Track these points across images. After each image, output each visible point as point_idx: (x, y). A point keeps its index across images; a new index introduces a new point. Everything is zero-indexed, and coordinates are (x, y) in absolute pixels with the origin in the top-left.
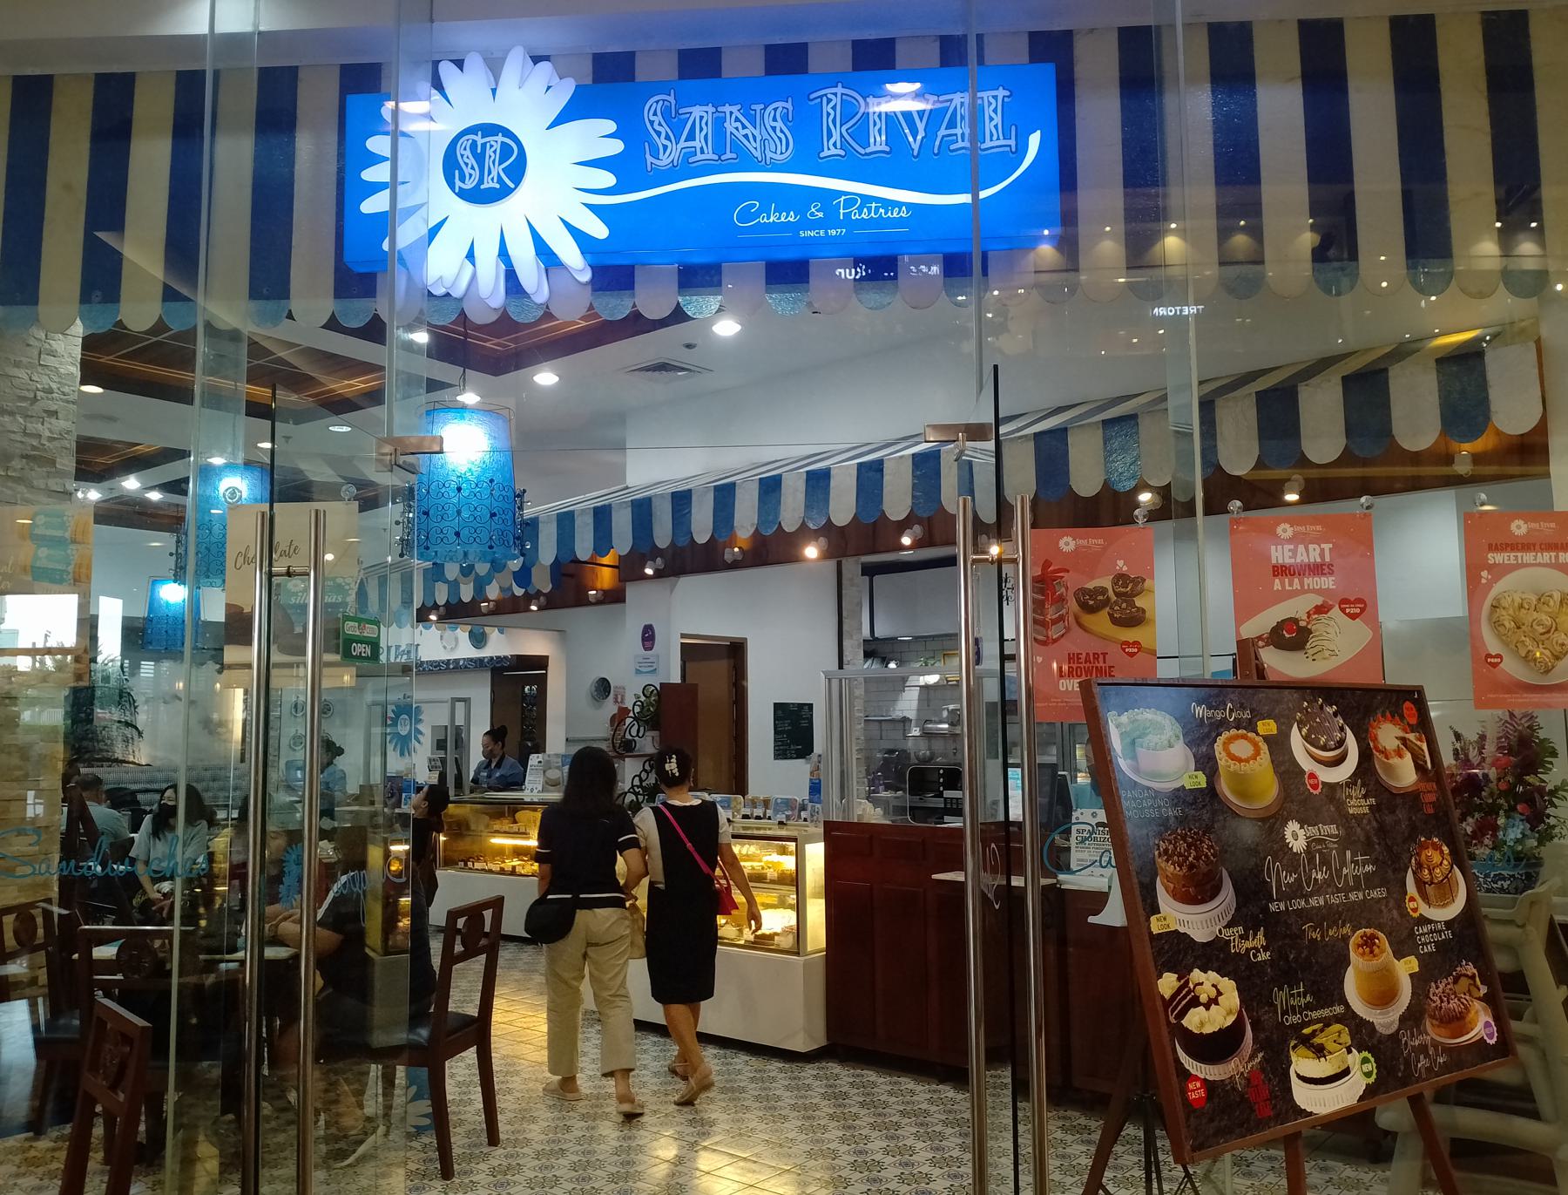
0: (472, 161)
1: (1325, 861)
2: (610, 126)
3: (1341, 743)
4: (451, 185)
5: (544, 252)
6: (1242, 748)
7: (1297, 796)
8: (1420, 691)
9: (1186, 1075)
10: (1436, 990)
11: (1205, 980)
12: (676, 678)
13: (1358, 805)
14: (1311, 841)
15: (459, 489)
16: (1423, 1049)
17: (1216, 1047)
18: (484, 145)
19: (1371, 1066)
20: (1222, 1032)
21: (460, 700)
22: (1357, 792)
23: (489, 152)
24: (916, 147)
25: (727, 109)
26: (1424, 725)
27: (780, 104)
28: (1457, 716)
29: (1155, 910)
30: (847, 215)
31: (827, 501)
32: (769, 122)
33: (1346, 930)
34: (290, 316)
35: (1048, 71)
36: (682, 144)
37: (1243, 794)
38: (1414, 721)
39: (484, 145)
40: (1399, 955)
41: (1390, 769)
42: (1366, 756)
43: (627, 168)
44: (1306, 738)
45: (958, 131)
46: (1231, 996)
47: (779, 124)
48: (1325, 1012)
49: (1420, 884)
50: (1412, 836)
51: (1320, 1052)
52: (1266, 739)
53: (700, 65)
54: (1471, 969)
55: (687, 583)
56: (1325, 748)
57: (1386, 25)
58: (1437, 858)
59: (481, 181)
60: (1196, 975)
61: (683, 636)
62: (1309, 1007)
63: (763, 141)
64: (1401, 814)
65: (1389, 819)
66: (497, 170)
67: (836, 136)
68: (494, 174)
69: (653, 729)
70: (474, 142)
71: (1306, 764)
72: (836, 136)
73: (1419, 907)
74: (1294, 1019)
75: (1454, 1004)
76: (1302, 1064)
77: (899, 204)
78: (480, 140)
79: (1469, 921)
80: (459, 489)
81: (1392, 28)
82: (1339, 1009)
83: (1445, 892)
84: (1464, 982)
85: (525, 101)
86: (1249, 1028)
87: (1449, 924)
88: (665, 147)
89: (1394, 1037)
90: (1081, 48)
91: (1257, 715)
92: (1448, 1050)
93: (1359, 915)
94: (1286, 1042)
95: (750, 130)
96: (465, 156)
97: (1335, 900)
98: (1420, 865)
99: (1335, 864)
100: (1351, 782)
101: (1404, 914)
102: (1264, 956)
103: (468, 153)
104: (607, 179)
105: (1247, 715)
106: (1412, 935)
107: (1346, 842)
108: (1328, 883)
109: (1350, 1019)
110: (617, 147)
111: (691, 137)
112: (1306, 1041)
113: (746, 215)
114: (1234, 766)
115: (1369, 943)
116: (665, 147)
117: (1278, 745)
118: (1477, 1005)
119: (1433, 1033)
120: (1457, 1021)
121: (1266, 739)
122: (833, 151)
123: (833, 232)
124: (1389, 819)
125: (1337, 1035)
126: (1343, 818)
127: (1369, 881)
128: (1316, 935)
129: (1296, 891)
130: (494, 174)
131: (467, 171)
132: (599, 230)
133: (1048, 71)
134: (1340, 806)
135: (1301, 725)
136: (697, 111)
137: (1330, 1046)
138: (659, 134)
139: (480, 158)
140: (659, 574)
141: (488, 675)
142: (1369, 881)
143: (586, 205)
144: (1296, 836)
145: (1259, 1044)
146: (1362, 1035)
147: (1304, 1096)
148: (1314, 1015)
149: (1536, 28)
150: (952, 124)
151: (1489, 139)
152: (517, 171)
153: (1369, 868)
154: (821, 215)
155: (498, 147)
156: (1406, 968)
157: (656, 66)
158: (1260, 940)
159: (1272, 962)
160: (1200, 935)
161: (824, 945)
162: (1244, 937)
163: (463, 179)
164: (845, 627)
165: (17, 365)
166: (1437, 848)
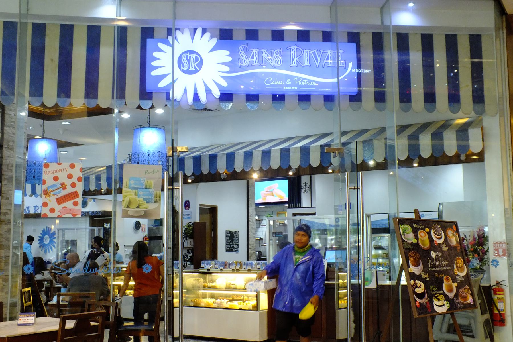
0: (186, 61)
1: (439, 260)
2: (228, 53)
3: (441, 234)
4: (180, 69)
5: (208, 92)
6: (423, 234)
7: (433, 246)
8: (456, 223)
9: (416, 301)
10: (461, 291)
11: (418, 283)
12: (198, 220)
13: (445, 248)
14: (436, 256)
15: (149, 155)
16: (458, 303)
17: (421, 296)
18: (190, 57)
19: (448, 305)
20: (421, 293)
21: (61, 229)
22: (445, 245)
23: (192, 59)
24: (318, 65)
25: (263, 50)
26: (457, 231)
27: (279, 50)
28: (466, 230)
29: (409, 267)
30: (298, 83)
31: (269, 160)
32: (275, 55)
33: (443, 275)
34: (126, 104)
35: (354, 45)
36: (250, 60)
37: (423, 245)
38: (455, 230)
39: (190, 57)
40: (453, 282)
41: (450, 241)
42: (446, 237)
43: (233, 65)
44: (434, 233)
45: (329, 61)
46: (423, 287)
47: (278, 56)
48: (439, 292)
49: (457, 267)
50: (455, 257)
51: (439, 300)
52: (427, 232)
53: (252, 35)
54: (468, 287)
55: (201, 185)
56: (438, 235)
57: (444, 37)
58: (460, 262)
59: (189, 68)
60: (417, 281)
61: (201, 205)
62: (437, 290)
63: (274, 61)
64: (453, 251)
65: (451, 252)
66: (194, 64)
67: (295, 60)
68: (193, 66)
69: (190, 238)
70: (187, 56)
71: (435, 239)
72: (295, 60)
73: (457, 272)
74: (434, 293)
75: (464, 294)
76: (436, 302)
77: (313, 81)
78: (189, 55)
79: (467, 276)
80: (149, 155)
81: (446, 38)
82: (442, 292)
83: (462, 270)
84: (466, 290)
85: (204, 44)
86: (426, 294)
87: (463, 277)
88: (245, 61)
89: (453, 299)
90: (362, 38)
91: (425, 227)
92: (463, 304)
93: (446, 272)
94: (432, 297)
95: (270, 57)
96: (184, 60)
97: (441, 269)
98: (457, 263)
99: (440, 261)
100: (443, 243)
101: (454, 274)
102: (428, 279)
103: (185, 59)
104: (227, 69)
105: (423, 227)
106: (456, 278)
107: (443, 256)
108: (439, 265)
109: (444, 294)
110: (230, 59)
111: (252, 58)
112: (436, 297)
113: (268, 82)
114: (421, 238)
115: (447, 278)
116: (245, 61)
117: (429, 234)
118: (469, 295)
119: (460, 300)
120: (465, 298)
121: (427, 232)
122: (294, 65)
123: (294, 88)
124: (451, 252)
125: (441, 297)
126: (442, 251)
127: (448, 265)
128: (437, 276)
129: (433, 266)
130: (193, 66)
131: (185, 64)
132: (224, 84)
133: (354, 45)
134: (441, 248)
135: (433, 229)
136: (254, 51)
137: (441, 299)
138: (243, 56)
139: (189, 61)
140: (193, 182)
141: (88, 219)
142: (448, 265)
143: (222, 77)
144: (433, 254)
145: (428, 297)
146: (447, 298)
147: (436, 308)
148: (438, 292)
149: (483, 39)
150: (328, 59)
151: (470, 70)
152: (200, 65)
153: (447, 263)
154: (290, 83)
155: (194, 57)
156: (455, 285)
157: (239, 34)
158: (427, 276)
159: (430, 280)
160: (417, 274)
161: (267, 308)
162: (424, 275)
163: (184, 67)
164: (250, 202)
165: (11, 110)
166: (460, 259)
